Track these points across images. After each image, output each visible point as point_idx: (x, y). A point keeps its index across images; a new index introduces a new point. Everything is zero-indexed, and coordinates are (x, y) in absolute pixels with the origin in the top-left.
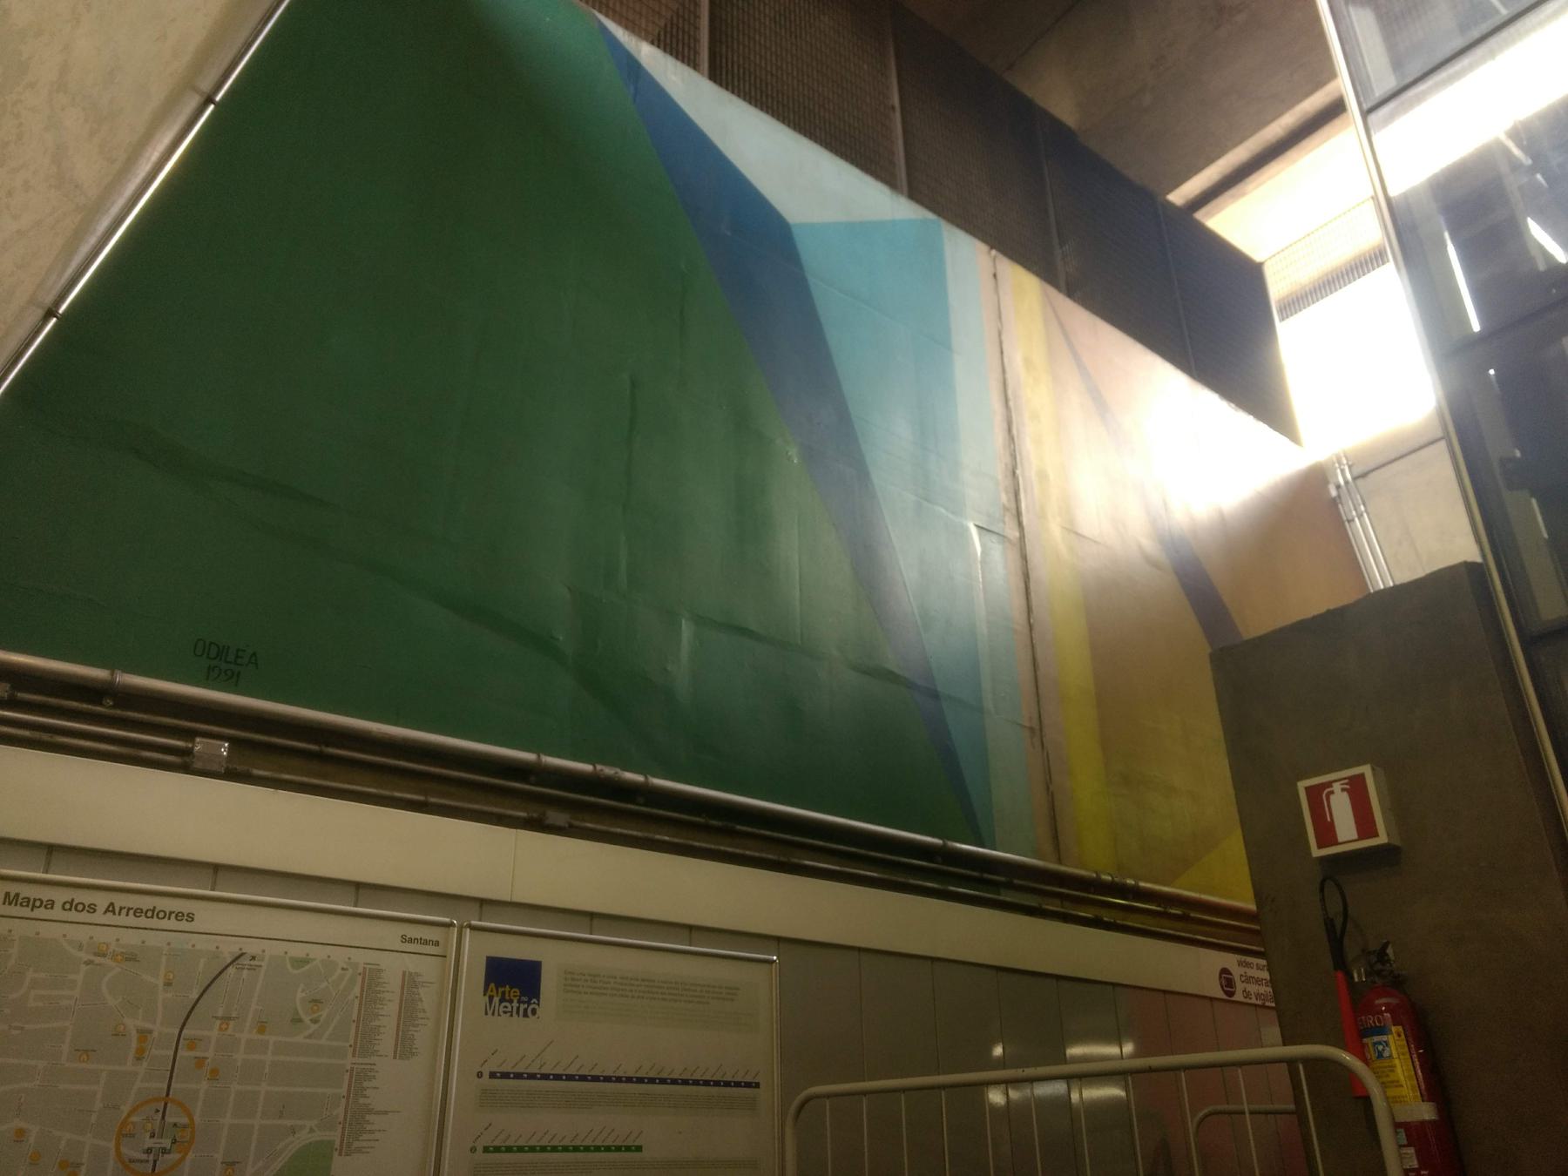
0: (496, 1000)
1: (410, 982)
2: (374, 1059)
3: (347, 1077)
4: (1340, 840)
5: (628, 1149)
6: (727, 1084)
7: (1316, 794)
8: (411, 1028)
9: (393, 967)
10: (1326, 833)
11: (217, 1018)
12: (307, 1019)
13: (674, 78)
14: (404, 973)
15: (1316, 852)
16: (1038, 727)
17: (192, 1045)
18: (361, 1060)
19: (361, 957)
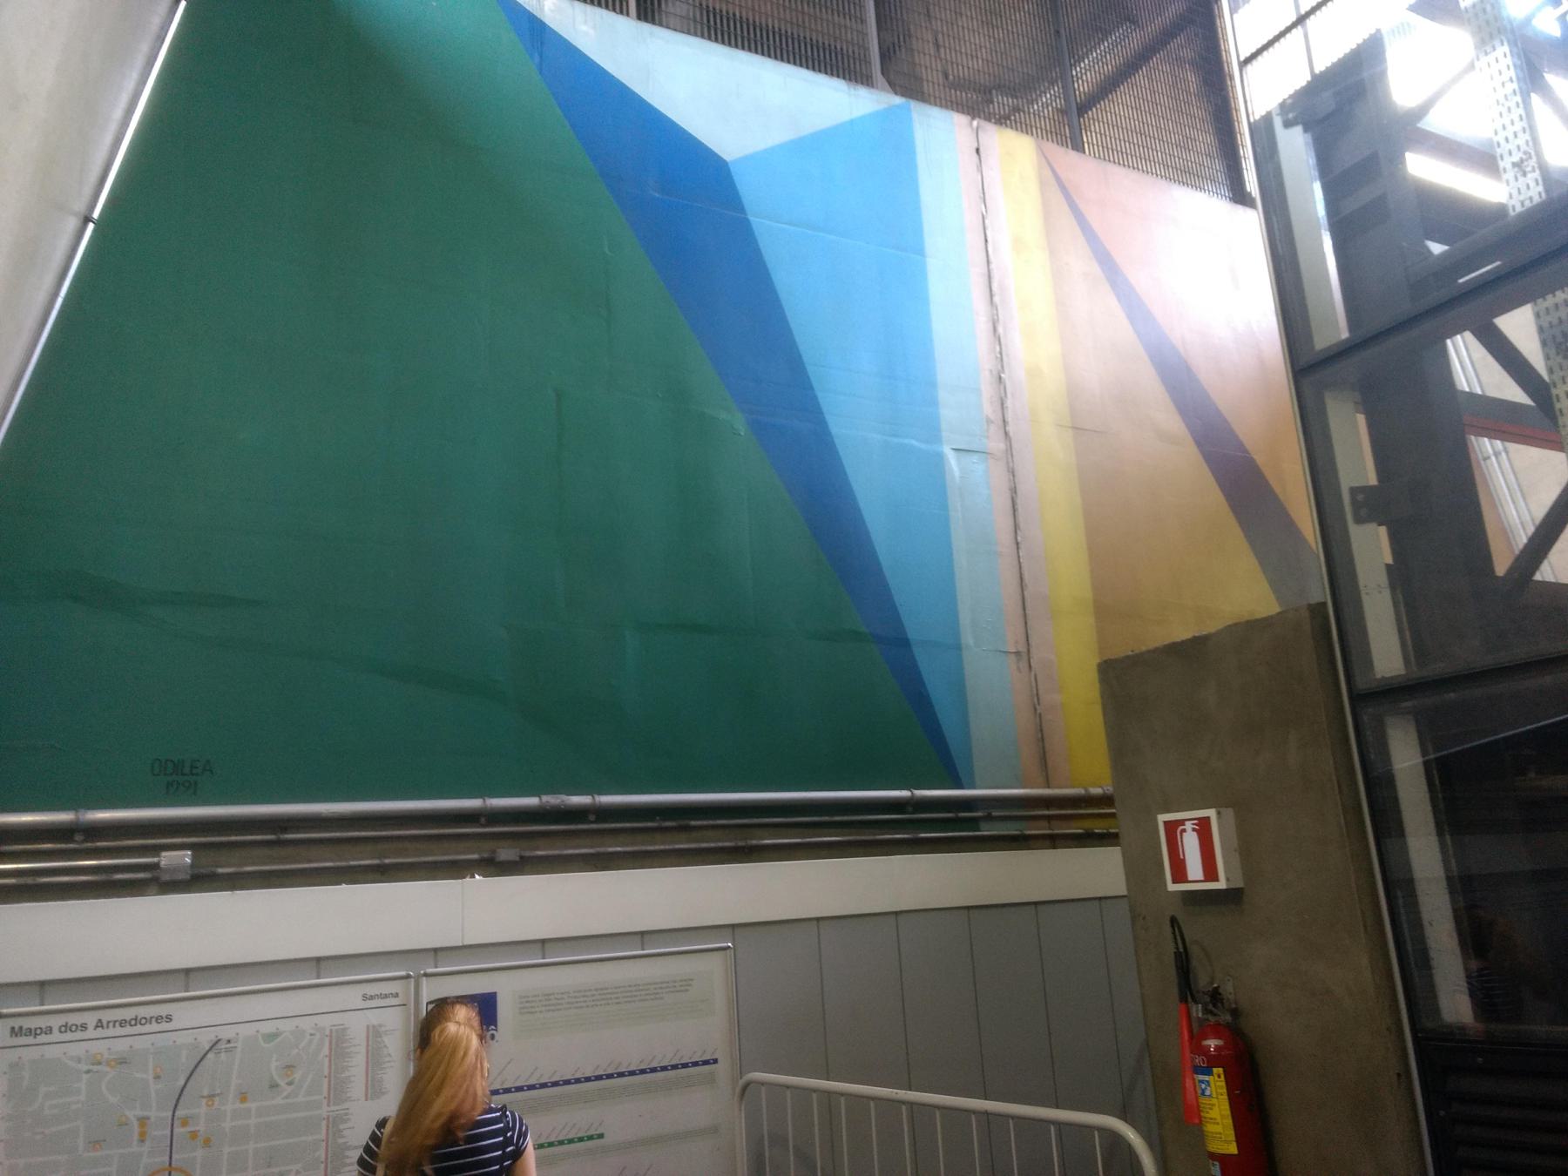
1: (374, 1033)
2: (346, 1105)
3: (324, 1123)
4: (1190, 878)
5: (591, 1138)
6: (685, 1066)
7: (1173, 828)
8: (380, 1072)
9: (357, 1026)
10: (1180, 874)
11: (203, 1097)
12: (282, 1083)
13: (584, 28)
14: (368, 1027)
15: (1172, 887)
16: (1025, 650)
18: (333, 1108)
19: (327, 1022)
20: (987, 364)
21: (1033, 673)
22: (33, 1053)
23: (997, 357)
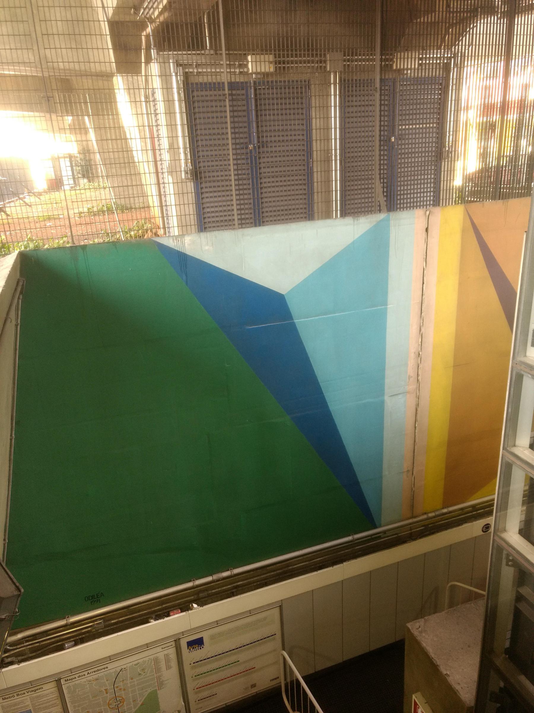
0: (191, 649)
1: (167, 656)
9: (161, 656)
12: (142, 673)
17: (117, 687)
19: (152, 657)
20: (413, 347)
21: (413, 477)
22: (73, 683)
23: (419, 345)
